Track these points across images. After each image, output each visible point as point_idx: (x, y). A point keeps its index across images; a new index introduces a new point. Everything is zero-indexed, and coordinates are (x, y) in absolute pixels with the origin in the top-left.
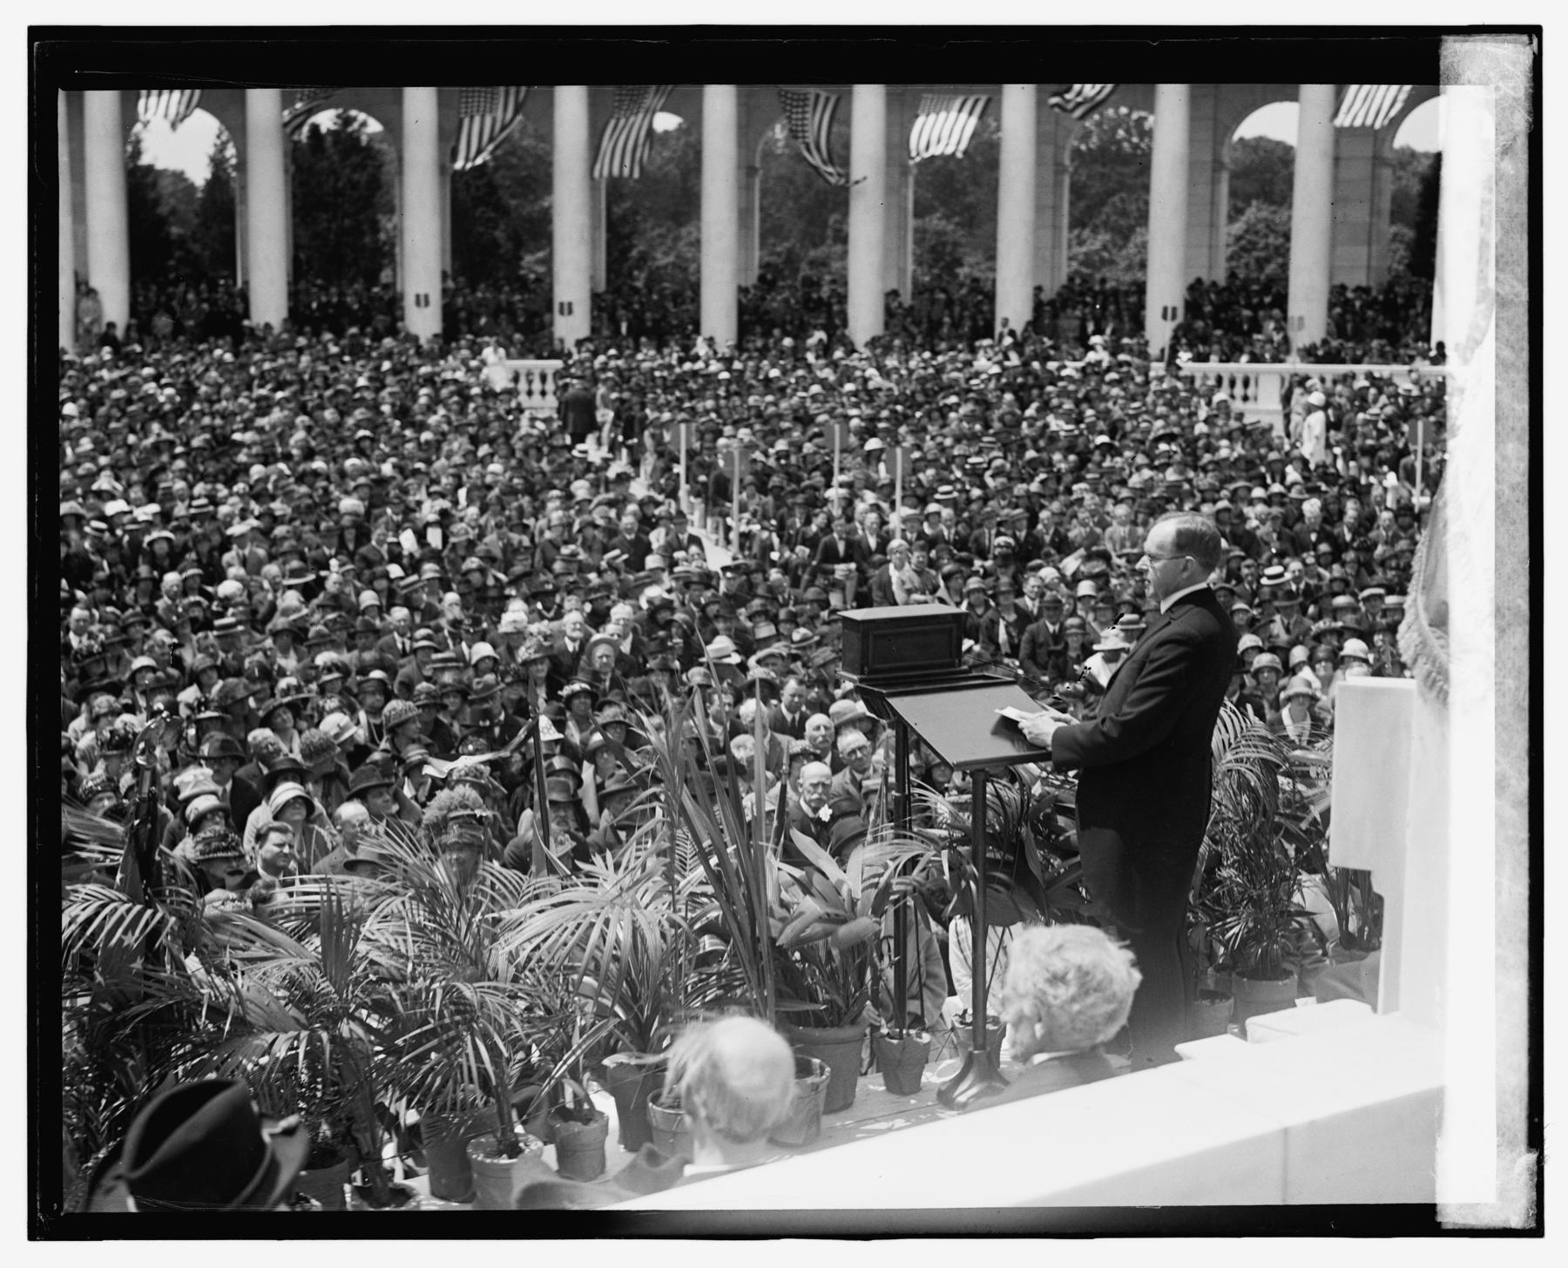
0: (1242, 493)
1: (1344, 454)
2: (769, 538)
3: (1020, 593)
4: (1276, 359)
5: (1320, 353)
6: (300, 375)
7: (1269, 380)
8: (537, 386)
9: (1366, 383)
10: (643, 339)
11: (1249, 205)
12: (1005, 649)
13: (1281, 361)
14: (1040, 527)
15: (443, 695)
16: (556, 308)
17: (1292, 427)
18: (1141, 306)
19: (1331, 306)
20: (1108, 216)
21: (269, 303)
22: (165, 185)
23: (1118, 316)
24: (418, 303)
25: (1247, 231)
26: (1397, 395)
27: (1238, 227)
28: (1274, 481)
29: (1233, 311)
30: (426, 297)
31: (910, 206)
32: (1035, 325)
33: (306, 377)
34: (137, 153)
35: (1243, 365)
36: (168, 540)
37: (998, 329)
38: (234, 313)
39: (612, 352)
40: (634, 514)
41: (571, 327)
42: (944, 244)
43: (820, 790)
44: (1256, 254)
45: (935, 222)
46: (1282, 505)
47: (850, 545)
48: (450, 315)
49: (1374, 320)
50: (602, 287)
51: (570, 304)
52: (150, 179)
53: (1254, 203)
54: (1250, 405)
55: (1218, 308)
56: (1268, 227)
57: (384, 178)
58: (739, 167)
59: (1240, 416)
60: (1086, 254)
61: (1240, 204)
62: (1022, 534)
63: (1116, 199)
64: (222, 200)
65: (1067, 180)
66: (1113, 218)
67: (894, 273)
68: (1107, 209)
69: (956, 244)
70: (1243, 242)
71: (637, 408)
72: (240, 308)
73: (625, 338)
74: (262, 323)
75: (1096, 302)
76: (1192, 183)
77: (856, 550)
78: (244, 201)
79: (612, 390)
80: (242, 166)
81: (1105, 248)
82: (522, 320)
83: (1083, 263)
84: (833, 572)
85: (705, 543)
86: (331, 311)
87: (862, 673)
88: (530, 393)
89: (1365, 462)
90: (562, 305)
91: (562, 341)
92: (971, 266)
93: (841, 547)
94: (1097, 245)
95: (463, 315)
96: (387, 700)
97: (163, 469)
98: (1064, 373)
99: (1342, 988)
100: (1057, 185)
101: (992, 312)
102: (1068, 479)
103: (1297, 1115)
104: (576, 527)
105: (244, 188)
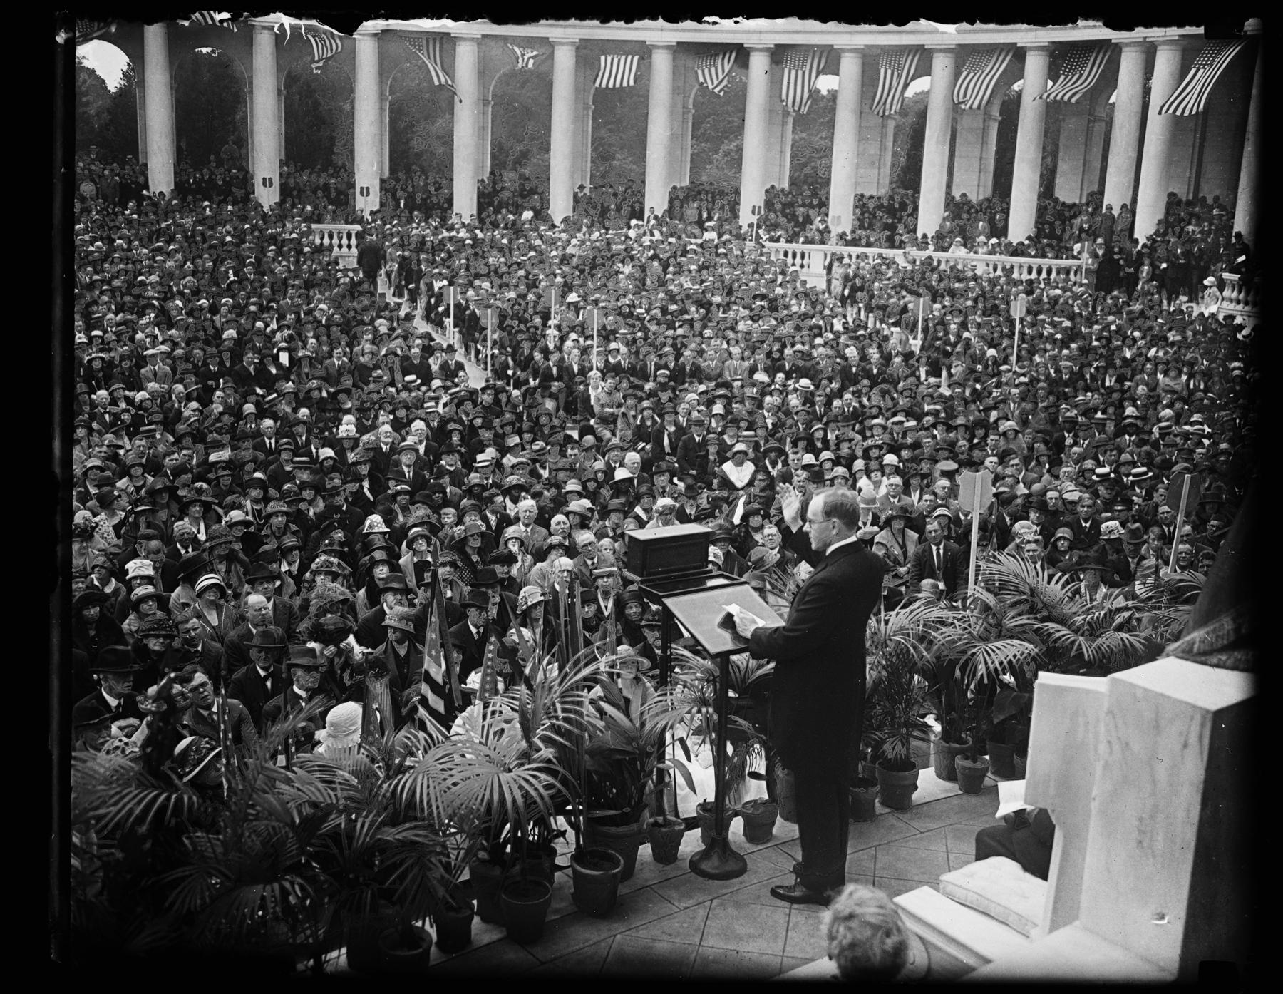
2: (506, 360)
4: (822, 242)
5: (849, 238)
8: (345, 241)
12: (667, 449)
16: (358, 191)
19: (856, 207)
21: (161, 178)
24: (264, 185)
29: (797, 206)
30: (270, 179)
32: (670, 212)
35: (798, 247)
37: (647, 214)
38: (137, 183)
41: (367, 204)
47: (560, 368)
50: (387, 174)
55: (785, 205)
72: (141, 180)
75: (707, 196)
77: (564, 370)
84: (550, 387)
88: (340, 246)
93: (555, 370)
101: (642, 204)
102: (698, 325)
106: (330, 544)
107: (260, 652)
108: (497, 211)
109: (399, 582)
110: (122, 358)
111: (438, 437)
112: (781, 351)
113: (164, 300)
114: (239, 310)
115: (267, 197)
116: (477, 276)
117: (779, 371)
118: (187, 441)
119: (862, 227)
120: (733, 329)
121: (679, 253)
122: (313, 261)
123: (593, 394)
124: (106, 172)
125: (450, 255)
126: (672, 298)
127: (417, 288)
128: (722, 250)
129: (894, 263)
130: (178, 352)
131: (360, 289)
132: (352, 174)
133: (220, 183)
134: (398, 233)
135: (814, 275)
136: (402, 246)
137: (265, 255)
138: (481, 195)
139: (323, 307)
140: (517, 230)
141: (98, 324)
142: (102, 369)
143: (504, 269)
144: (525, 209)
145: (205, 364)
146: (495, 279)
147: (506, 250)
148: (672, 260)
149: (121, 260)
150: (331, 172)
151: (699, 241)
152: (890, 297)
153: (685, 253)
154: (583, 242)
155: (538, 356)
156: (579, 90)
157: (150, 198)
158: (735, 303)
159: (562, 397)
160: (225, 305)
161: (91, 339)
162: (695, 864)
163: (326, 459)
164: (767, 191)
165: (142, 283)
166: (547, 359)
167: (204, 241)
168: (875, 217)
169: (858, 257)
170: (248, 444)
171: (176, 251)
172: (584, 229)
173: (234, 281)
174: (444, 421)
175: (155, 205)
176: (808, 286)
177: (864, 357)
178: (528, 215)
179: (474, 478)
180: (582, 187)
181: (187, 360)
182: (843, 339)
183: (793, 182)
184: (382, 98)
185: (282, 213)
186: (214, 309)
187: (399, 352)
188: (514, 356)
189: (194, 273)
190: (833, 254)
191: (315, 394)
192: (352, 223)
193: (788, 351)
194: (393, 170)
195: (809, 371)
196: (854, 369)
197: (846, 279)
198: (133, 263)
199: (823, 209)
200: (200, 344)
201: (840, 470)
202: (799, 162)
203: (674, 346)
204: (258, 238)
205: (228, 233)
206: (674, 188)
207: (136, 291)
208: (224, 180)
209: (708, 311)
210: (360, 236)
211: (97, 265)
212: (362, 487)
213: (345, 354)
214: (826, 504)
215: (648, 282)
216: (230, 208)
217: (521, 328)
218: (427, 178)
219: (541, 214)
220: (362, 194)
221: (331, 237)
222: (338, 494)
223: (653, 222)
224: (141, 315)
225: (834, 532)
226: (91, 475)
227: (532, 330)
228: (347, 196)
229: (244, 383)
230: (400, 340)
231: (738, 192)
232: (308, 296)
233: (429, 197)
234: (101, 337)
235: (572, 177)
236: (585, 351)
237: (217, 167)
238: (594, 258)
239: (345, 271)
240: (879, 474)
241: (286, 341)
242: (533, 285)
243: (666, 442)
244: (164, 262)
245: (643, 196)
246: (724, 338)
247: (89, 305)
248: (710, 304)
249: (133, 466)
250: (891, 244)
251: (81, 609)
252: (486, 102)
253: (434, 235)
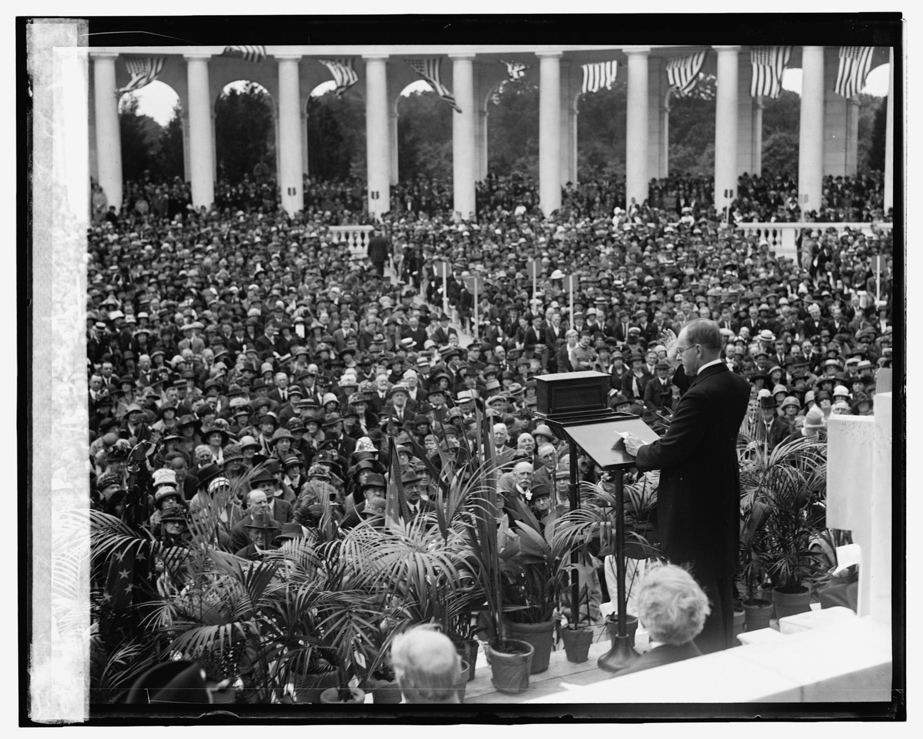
2: (496, 329)
4: (793, 220)
5: (818, 215)
7: (788, 235)
12: (636, 394)
18: (712, 189)
19: (824, 188)
21: (203, 194)
24: (289, 193)
29: (767, 191)
30: (294, 189)
32: (650, 201)
35: (772, 225)
37: (629, 203)
38: (183, 199)
41: (378, 206)
47: (543, 332)
50: (396, 181)
54: (778, 246)
55: (757, 190)
69: (603, 154)
72: (186, 196)
75: (686, 184)
84: (534, 349)
89: (847, 280)
93: (538, 334)
99: (837, 600)
101: (624, 195)
106: (323, 457)
107: (257, 533)
108: (493, 208)
109: (379, 481)
110: (163, 333)
111: (430, 384)
112: (746, 310)
113: (202, 289)
114: (265, 295)
115: (292, 205)
116: (473, 260)
118: (214, 391)
119: (831, 205)
120: (703, 294)
121: (657, 235)
122: (329, 254)
123: (570, 350)
124: (158, 191)
125: (449, 245)
126: (647, 271)
127: (420, 274)
128: (697, 231)
129: (861, 234)
130: (210, 328)
131: (369, 274)
132: (364, 182)
133: (252, 195)
134: (404, 229)
136: (407, 239)
138: (478, 195)
139: (335, 290)
140: (511, 222)
141: (146, 308)
142: (147, 342)
143: (496, 253)
144: (518, 204)
145: (233, 336)
146: (489, 264)
147: (499, 238)
148: (650, 241)
149: (167, 259)
150: (347, 182)
151: (676, 225)
152: (855, 263)
153: (662, 233)
154: (569, 229)
155: (523, 322)
156: (565, 99)
157: (193, 211)
158: (707, 273)
159: (545, 358)
160: (252, 290)
161: (138, 320)
162: (602, 664)
164: (740, 178)
165: (184, 277)
166: (530, 324)
167: (237, 241)
168: (843, 195)
169: (827, 232)
170: (264, 392)
171: (213, 251)
172: (571, 219)
173: (260, 273)
174: (434, 372)
175: (197, 216)
176: (776, 257)
177: (825, 312)
178: (520, 210)
179: (455, 411)
180: (569, 184)
181: (218, 334)
182: (806, 299)
183: (764, 170)
184: (390, 114)
185: (304, 218)
186: (243, 295)
187: (399, 321)
188: (503, 324)
189: (227, 267)
190: (802, 229)
191: (324, 355)
192: (365, 224)
194: (401, 178)
195: (769, 320)
196: (817, 324)
197: (815, 251)
198: (177, 261)
199: (794, 191)
200: (229, 321)
201: (791, 400)
202: (770, 153)
203: (648, 310)
204: (283, 238)
205: (258, 235)
206: (654, 180)
207: (177, 282)
208: (256, 193)
209: (681, 282)
210: (371, 234)
211: (147, 263)
212: (358, 423)
213: (352, 326)
215: (627, 259)
216: (260, 216)
217: (505, 300)
218: (431, 183)
219: (532, 209)
220: (373, 197)
221: (347, 236)
222: (335, 425)
223: (634, 210)
224: (181, 299)
226: (133, 418)
227: (519, 302)
228: (361, 202)
229: (263, 350)
231: (712, 180)
232: (323, 282)
233: (433, 199)
234: (147, 319)
235: (560, 175)
236: (565, 317)
237: (250, 182)
238: (579, 243)
239: (356, 261)
240: (828, 402)
241: (301, 316)
242: (521, 266)
243: (635, 386)
244: (202, 259)
245: (625, 188)
246: (695, 302)
247: (138, 294)
248: (683, 275)
249: (166, 410)
250: (859, 218)
252: (481, 113)
253: (436, 229)
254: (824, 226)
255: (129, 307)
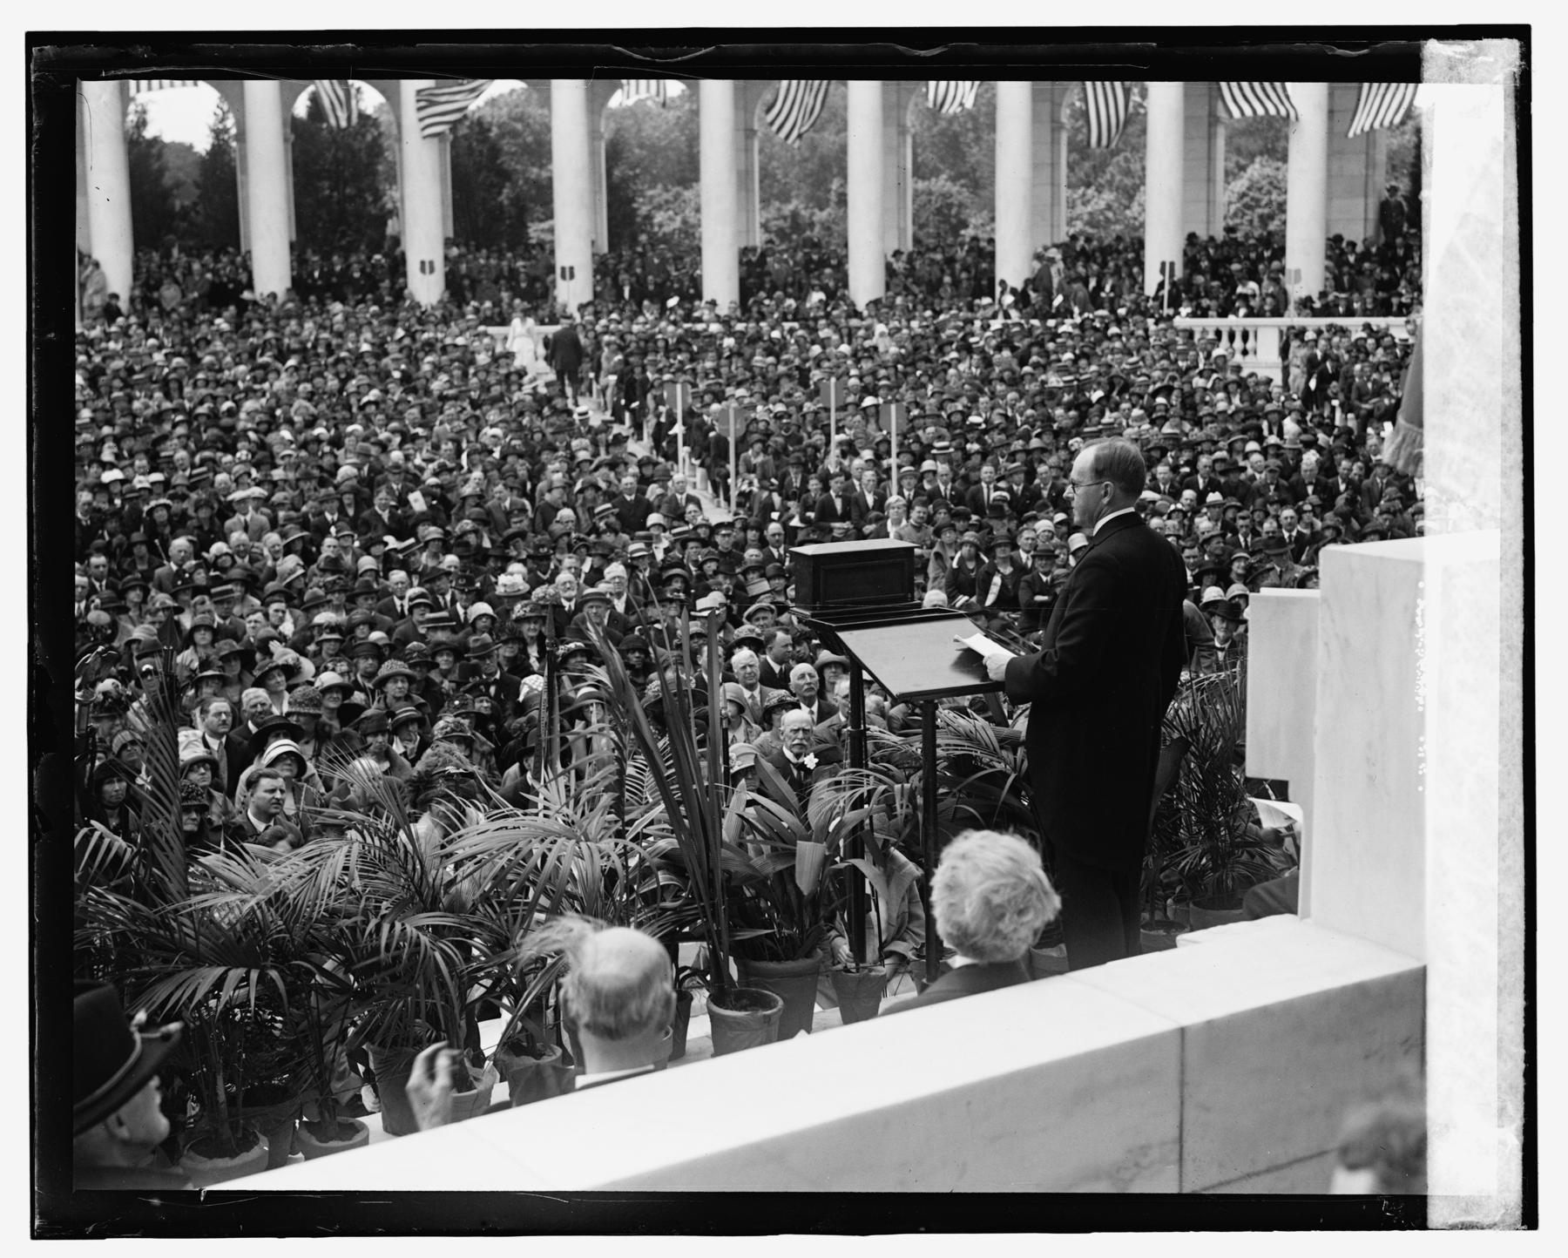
0: (1238, 446)
1: (1341, 405)
2: (770, 497)
3: (1015, 547)
4: (1278, 312)
5: (1317, 305)
6: (303, 343)
7: (1268, 334)
9: (1364, 335)
10: (646, 303)
11: (1252, 162)
13: (1281, 315)
14: (1037, 481)
15: (434, 655)
16: (558, 271)
17: (1291, 379)
20: (1113, 176)
21: (271, 270)
22: (171, 160)
23: (1117, 272)
24: (423, 270)
25: (1249, 189)
26: (1394, 345)
27: (1240, 185)
28: (1271, 432)
30: (431, 263)
31: (909, 166)
33: (309, 345)
34: (142, 124)
35: (1236, 321)
36: (167, 507)
39: (614, 316)
40: (634, 475)
41: (573, 293)
42: (950, 206)
43: (800, 734)
44: (1259, 211)
45: (941, 183)
46: (1277, 456)
48: (454, 284)
49: (1372, 271)
50: (605, 249)
51: (572, 269)
52: (154, 151)
53: (1258, 159)
54: (1250, 357)
56: (1271, 183)
57: (386, 143)
58: (736, 129)
59: (1238, 369)
60: (1090, 214)
61: (1243, 162)
62: (1018, 489)
63: (1120, 158)
64: (221, 171)
65: (1064, 137)
66: (1118, 178)
67: (894, 233)
68: (1110, 169)
69: (961, 205)
70: (1246, 199)
71: (638, 370)
72: (243, 277)
73: (627, 303)
74: (266, 293)
76: (1188, 137)
78: (245, 171)
79: (615, 353)
80: (241, 136)
81: (1109, 207)
82: (523, 285)
83: (1088, 223)
85: (704, 503)
86: (334, 280)
87: (814, 609)
90: (563, 269)
91: (565, 306)
92: (976, 227)
93: (838, 504)
94: (1102, 205)
95: (466, 282)
96: (381, 663)
97: (165, 438)
98: (1061, 330)
100: (1055, 142)
103: (1192, 1017)
104: (578, 486)
105: (244, 158)
112: (1192, 463)
115: (426, 289)
117: (1188, 487)
119: (1339, 287)
127: (643, 406)
133: (357, 275)
135: (1263, 357)
137: (418, 369)
144: (813, 288)
149: (207, 382)
157: (255, 303)
160: (351, 433)
163: (481, 616)
166: (826, 488)
176: (1244, 374)
178: (817, 297)
180: (897, 254)
186: (337, 442)
193: (1204, 460)
197: (1312, 365)
208: (362, 271)
214: (1097, 459)
217: (792, 453)
219: (837, 291)
220: (563, 277)
222: (489, 656)
225: (1106, 500)
230: (604, 470)
235: (882, 239)
250: (1384, 309)
251: (101, 783)
254: (1323, 322)
255: (141, 462)
